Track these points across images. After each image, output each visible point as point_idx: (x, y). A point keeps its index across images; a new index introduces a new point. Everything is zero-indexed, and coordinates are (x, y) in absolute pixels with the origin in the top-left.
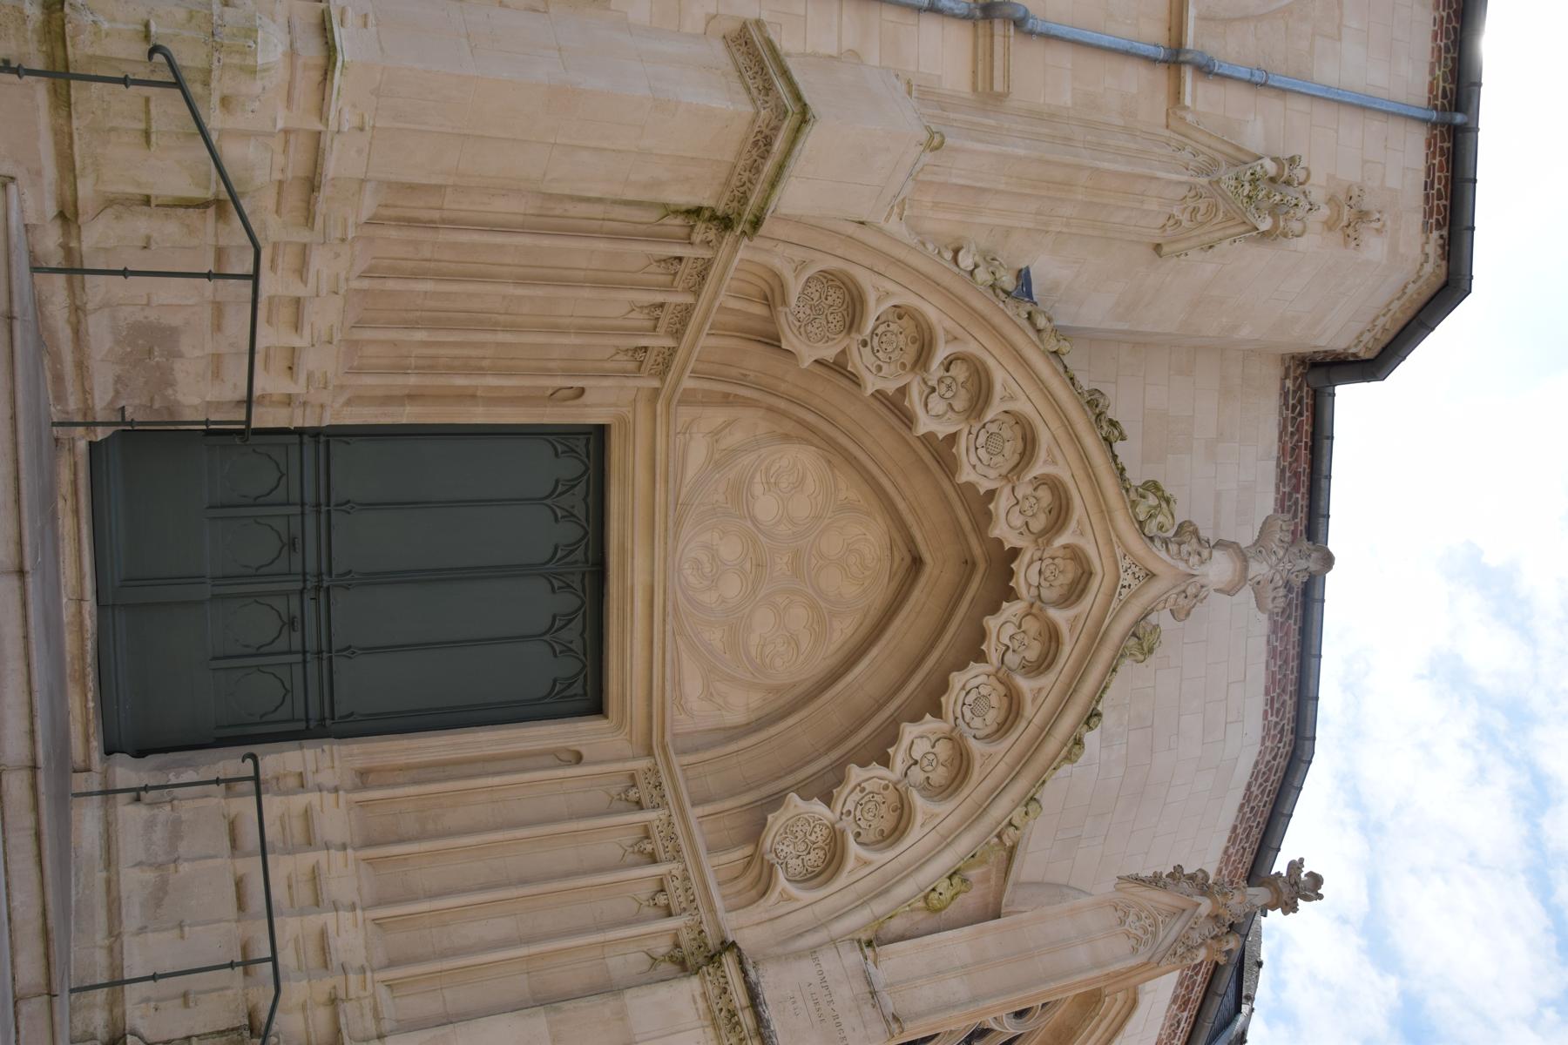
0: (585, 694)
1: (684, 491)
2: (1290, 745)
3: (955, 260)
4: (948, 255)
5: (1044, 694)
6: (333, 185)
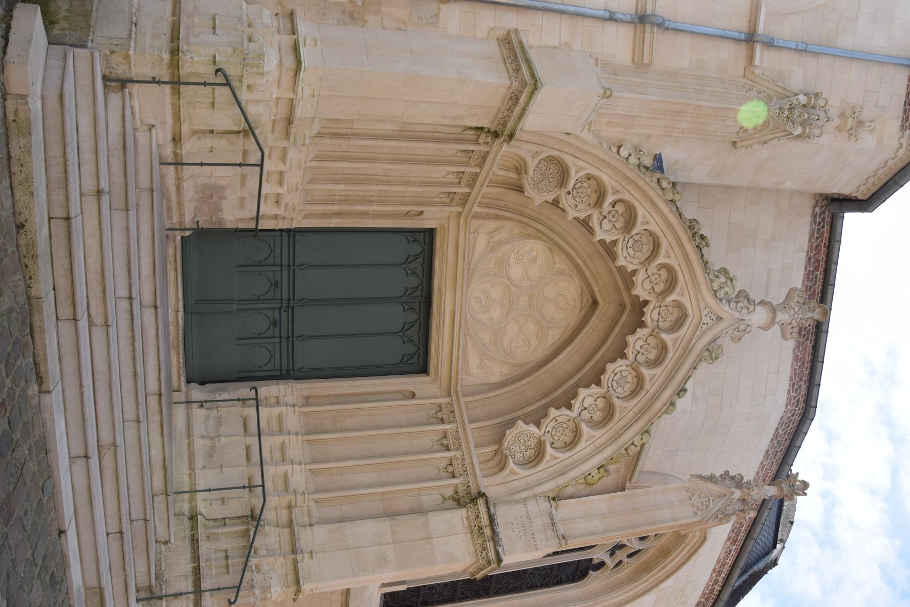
0: (419, 363)
1: (473, 262)
2: (802, 409)
3: (618, 151)
4: (614, 150)
5: (656, 377)
6: (299, 120)
